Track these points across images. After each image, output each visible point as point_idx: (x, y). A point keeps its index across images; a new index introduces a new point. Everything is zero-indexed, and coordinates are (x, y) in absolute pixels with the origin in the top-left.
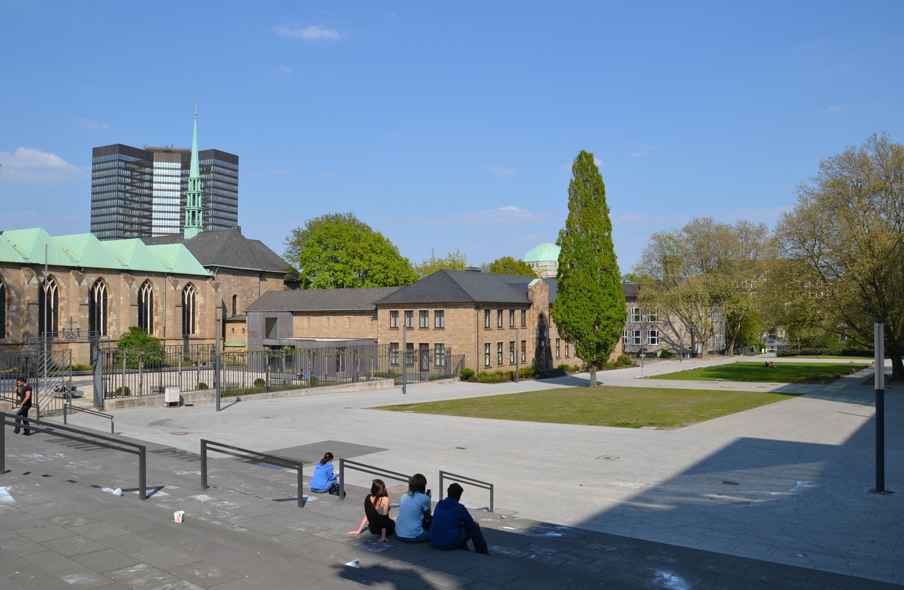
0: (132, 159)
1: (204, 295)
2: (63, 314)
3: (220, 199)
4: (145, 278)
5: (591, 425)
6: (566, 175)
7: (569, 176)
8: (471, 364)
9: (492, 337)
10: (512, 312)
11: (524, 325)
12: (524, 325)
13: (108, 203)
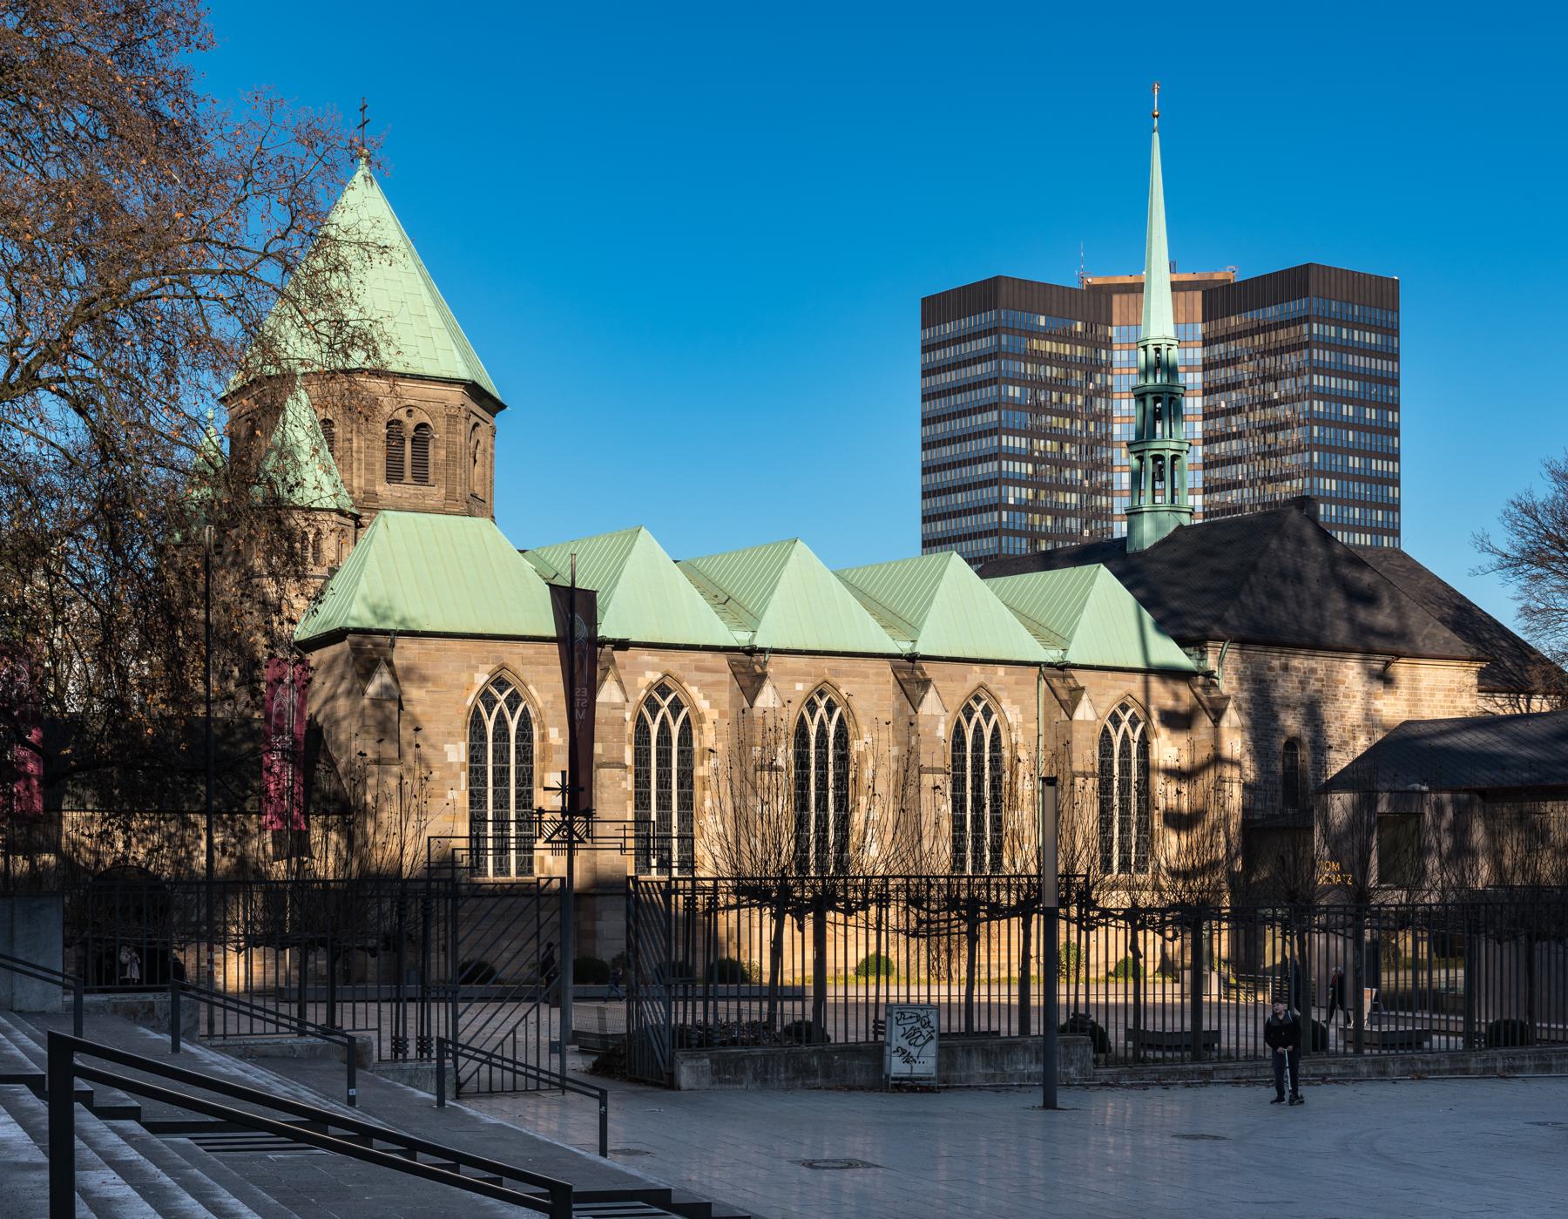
2: (708, 803)
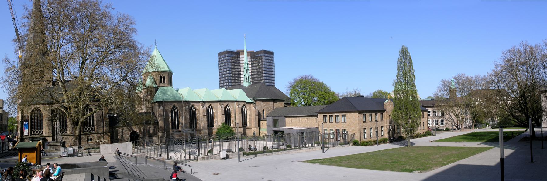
0: (232, 55)
1: (250, 110)
3: (267, 69)
4: (227, 103)
5: (391, 171)
6: (397, 56)
7: (398, 56)
8: (357, 138)
9: (367, 125)
10: (376, 115)
11: (382, 120)
12: (382, 120)
13: (225, 73)
